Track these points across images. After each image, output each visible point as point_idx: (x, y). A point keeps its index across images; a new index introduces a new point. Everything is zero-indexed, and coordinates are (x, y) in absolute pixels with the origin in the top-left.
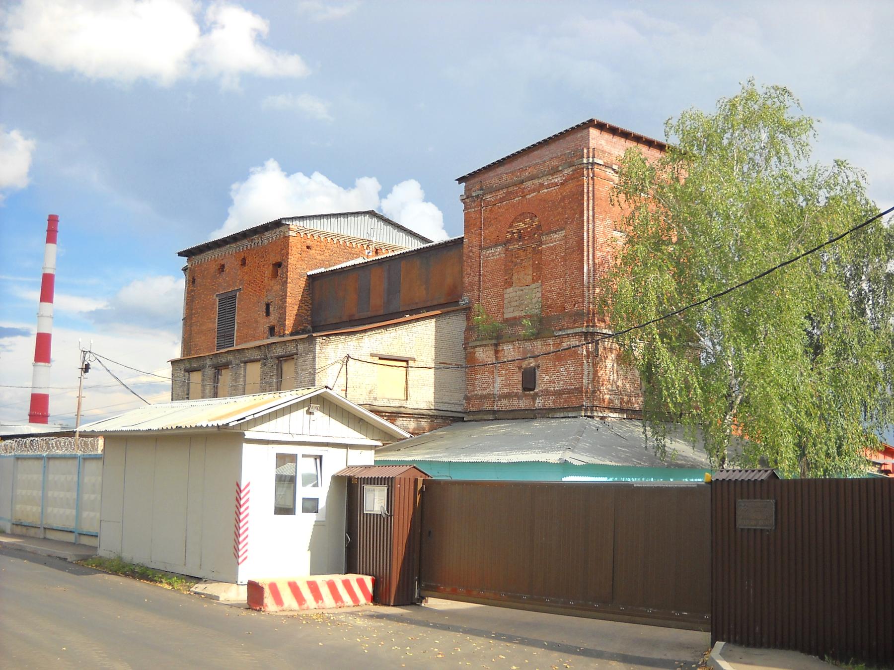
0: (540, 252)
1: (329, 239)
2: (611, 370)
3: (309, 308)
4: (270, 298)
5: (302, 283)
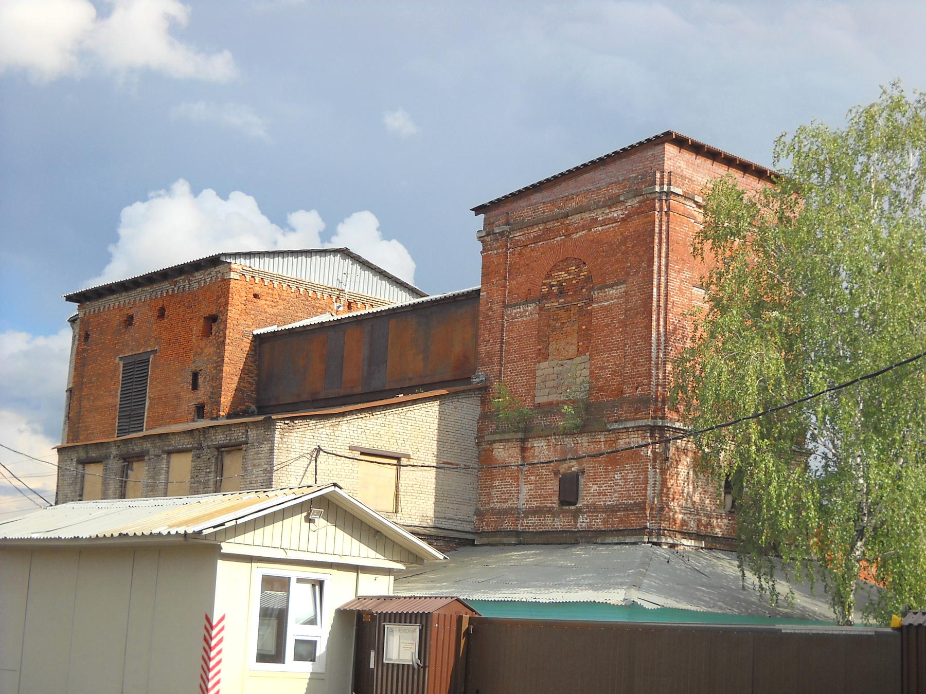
0: (590, 313)
1: (285, 285)
2: (686, 479)
3: (255, 380)
4: (199, 363)
5: (246, 345)
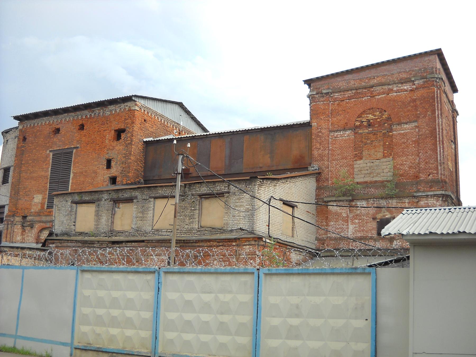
5: (140, 146)
